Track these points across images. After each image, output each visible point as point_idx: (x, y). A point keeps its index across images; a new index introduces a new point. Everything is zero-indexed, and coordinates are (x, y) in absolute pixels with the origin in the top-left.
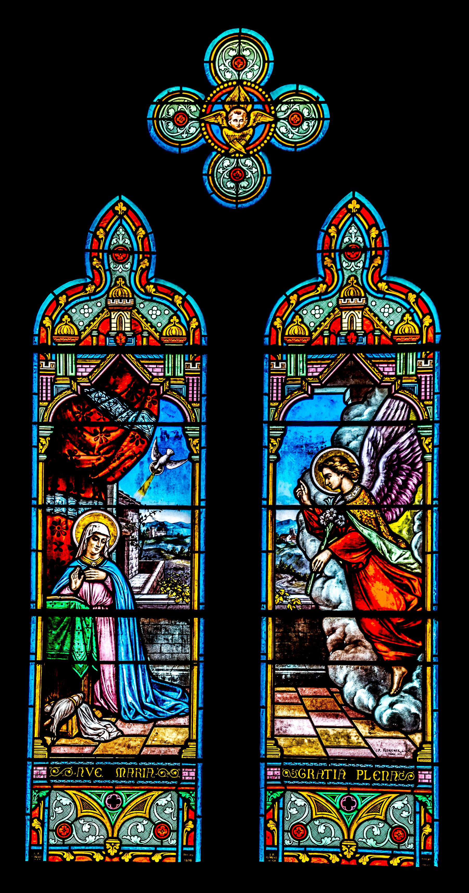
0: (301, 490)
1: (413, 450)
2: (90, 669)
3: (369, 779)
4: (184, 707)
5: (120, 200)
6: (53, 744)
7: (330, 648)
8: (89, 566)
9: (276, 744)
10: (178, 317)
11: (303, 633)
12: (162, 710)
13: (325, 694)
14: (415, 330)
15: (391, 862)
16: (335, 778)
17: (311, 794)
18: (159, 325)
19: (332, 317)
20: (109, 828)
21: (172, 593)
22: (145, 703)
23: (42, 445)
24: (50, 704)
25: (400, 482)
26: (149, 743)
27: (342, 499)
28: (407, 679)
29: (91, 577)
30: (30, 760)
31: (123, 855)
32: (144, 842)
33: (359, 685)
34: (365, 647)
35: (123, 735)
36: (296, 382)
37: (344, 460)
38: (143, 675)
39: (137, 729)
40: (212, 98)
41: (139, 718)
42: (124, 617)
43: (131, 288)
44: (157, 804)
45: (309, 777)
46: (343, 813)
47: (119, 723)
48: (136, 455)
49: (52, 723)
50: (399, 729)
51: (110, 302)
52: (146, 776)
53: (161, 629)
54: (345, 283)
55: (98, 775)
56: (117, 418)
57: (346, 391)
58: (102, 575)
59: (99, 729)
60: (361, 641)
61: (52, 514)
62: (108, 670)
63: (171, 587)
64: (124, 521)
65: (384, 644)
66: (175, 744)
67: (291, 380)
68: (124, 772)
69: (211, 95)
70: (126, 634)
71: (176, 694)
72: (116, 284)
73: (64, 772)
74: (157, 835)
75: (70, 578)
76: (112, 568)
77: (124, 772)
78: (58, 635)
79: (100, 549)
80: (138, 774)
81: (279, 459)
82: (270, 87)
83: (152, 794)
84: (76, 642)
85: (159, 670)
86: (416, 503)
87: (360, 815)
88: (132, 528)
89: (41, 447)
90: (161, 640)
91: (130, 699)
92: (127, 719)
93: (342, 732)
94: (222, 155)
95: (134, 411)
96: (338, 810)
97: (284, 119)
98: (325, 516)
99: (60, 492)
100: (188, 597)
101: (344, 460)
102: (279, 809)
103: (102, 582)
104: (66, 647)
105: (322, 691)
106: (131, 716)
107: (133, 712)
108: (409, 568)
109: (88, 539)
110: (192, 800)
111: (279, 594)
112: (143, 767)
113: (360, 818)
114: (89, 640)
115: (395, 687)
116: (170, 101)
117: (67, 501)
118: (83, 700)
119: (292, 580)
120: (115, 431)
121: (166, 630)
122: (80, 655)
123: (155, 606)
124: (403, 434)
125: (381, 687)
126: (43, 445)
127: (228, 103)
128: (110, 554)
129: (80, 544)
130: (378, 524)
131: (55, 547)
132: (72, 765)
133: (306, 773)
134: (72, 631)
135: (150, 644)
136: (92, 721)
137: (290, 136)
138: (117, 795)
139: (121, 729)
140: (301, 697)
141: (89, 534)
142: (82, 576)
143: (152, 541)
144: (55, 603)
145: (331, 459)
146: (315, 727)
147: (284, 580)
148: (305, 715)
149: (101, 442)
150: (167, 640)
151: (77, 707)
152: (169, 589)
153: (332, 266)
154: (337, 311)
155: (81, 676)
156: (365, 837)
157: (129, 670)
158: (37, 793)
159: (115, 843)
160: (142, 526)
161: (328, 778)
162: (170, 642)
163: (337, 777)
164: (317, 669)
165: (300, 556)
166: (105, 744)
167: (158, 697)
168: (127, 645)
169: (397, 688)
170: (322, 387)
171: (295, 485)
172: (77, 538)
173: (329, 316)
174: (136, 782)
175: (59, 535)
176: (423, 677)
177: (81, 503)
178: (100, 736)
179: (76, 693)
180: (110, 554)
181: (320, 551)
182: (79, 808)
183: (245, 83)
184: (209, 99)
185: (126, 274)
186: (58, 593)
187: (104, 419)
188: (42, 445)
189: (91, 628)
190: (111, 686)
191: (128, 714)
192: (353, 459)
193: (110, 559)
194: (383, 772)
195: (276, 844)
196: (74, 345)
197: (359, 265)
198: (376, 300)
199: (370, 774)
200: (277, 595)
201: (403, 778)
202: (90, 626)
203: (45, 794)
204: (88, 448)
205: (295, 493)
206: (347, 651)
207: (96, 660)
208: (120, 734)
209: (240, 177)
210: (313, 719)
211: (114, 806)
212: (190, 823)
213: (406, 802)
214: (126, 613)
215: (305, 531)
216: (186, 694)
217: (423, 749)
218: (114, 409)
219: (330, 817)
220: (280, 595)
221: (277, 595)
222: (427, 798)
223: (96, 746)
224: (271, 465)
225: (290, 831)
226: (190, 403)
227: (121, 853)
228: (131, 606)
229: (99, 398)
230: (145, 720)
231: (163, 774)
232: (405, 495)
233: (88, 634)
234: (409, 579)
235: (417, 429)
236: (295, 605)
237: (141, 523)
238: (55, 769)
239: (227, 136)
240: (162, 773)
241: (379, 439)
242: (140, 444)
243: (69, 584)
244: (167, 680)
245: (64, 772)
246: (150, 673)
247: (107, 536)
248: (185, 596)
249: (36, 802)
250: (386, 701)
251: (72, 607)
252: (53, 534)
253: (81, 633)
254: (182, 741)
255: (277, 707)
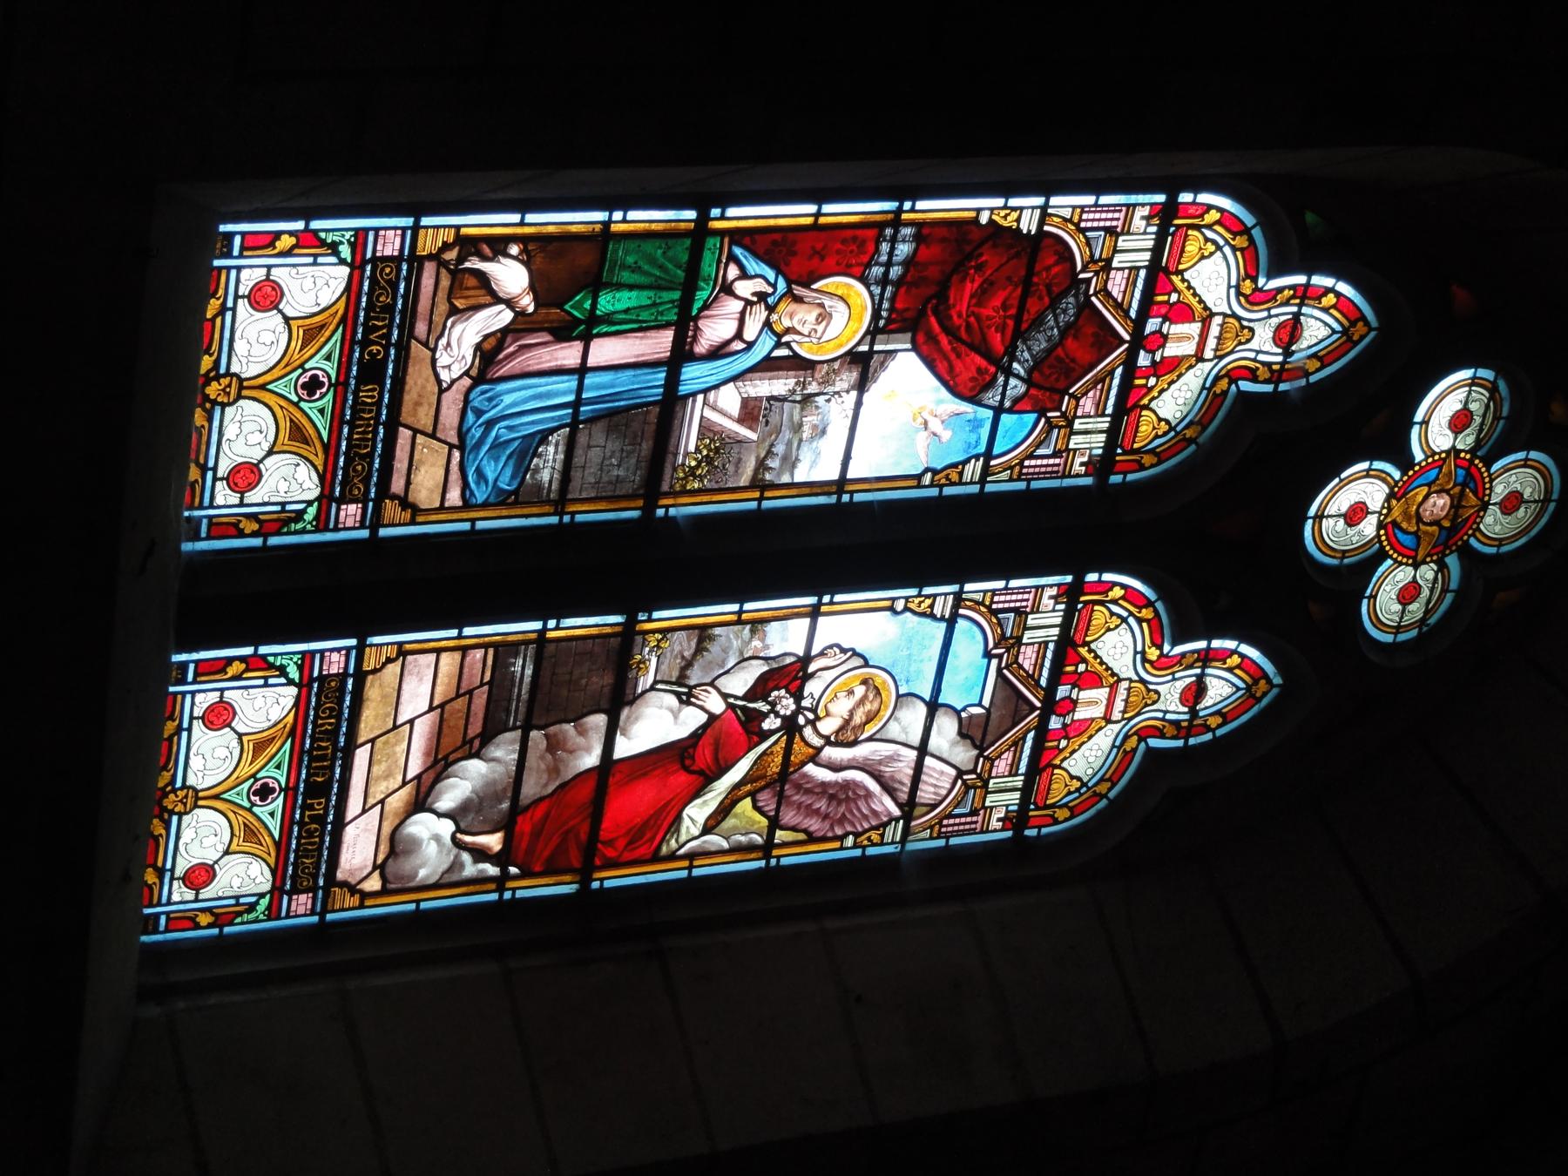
0: (835, 655)
1: (866, 817)
2: (578, 322)
3: (307, 820)
4: (480, 495)
5: (1371, 329)
6: (442, 264)
7: (552, 729)
8: (771, 309)
9: (389, 660)
10: (1165, 434)
11: (587, 685)
12: (480, 457)
13: (469, 731)
14: (1053, 798)
15: (150, 870)
16: (314, 765)
17: (287, 729)
18: (1072, 763)
19: (1105, 674)
20: (261, 381)
21: (695, 459)
22: (497, 427)
23: (1006, 215)
24: (521, 253)
25: (817, 806)
26: (420, 439)
27: (808, 722)
28: (480, 854)
29: (750, 314)
30: (417, 222)
31: (205, 410)
32: (225, 446)
33: (479, 783)
34: (546, 785)
35: (441, 391)
36: (1016, 630)
37: (870, 718)
38: (553, 419)
39: (450, 415)
40: (1476, 466)
41: (470, 417)
42: (667, 379)
43: (1232, 352)
44: (298, 465)
45: (320, 722)
46: (246, 785)
47: (467, 382)
48: (953, 378)
49: (485, 259)
50: (393, 852)
51: (1218, 320)
52: (357, 439)
53: (633, 445)
54: (1151, 687)
55: (370, 353)
56: (1024, 342)
57: (983, 707)
58: (749, 334)
59: (459, 347)
60: (557, 778)
61: (879, 238)
62: (569, 354)
63: (707, 456)
64: (842, 365)
65: (547, 815)
66: (411, 486)
67: (1020, 621)
68: (369, 400)
69: (1480, 465)
70: (633, 384)
71: (507, 480)
72: (1243, 328)
73: (384, 288)
74: (236, 470)
75: (757, 276)
76: (761, 351)
77: (369, 400)
78: (652, 261)
79: (799, 328)
80: (361, 426)
81: (896, 613)
82: (1466, 553)
83: (320, 454)
84: (634, 294)
85: (557, 445)
86: (523, 647)
87: (240, 812)
88: (826, 381)
89: (1003, 213)
90: (614, 445)
91: (508, 399)
92: (472, 396)
93: (397, 766)
94: (1391, 488)
95: (1030, 372)
96: (254, 776)
97: (1415, 576)
98: (783, 697)
99: (916, 251)
100: (684, 486)
101: (870, 718)
102: (266, 678)
103: (739, 335)
104: (626, 276)
105: (476, 728)
106: (476, 403)
107: (485, 406)
108: (672, 836)
109: (822, 305)
110: (300, 526)
111: (662, 639)
112: (376, 432)
113: (235, 813)
114: (634, 317)
115: (468, 839)
116: (1491, 404)
117: (899, 264)
118: (520, 314)
119: (683, 657)
120: (1003, 341)
121: (629, 453)
122: (607, 302)
123: (677, 433)
124: (895, 800)
125: (470, 818)
126: (1005, 217)
127: (1462, 493)
128: (788, 345)
129: (816, 291)
130: (753, 781)
131: (819, 246)
132: (395, 303)
133: (329, 717)
134: (656, 287)
135: (609, 426)
136: (477, 333)
137: (1388, 589)
138: (324, 390)
139: (454, 387)
140: (470, 692)
141: (831, 307)
142: (755, 299)
143: (796, 417)
144: (713, 253)
145: (878, 693)
146: (411, 722)
147: (685, 644)
148: (436, 703)
149: (988, 318)
150: (611, 457)
151: (509, 303)
152: (705, 452)
153: (1181, 665)
154: (1112, 680)
155: (567, 307)
156: (199, 825)
157: (564, 393)
158: (348, 241)
159: (229, 394)
160: (827, 397)
161: (315, 753)
162: (607, 462)
163: (316, 768)
164: (515, 716)
165: (722, 665)
166: (428, 361)
167: (505, 449)
168: (613, 386)
169: (466, 843)
170: (999, 670)
171: (846, 646)
172: (827, 285)
173: (1108, 668)
174: (348, 422)
175: (838, 252)
176: (480, 881)
177: (889, 289)
178: (446, 349)
179: (536, 299)
180: (788, 345)
181: (725, 696)
182: (308, 321)
183: (1410, 561)
184: (1477, 461)
185: (1254, 345)
186: (732, 258)
187: (1027, 321)
188: (1006, 215)
189: (656, 320)
190: (538, 364)
191: (480, 398)
192: (870, 730)
193: (778, 345)
194: (317, 840)
195: (198, 679)
196: (1163, 265)
197: (1173, 704)
198: (1113, 736)
199: (313, 819)
200: (660, 637)
201: (303, 872)
202: (659, 318)
203: (343, 256)
204: (981, 296)
205: (831, 647)
206: (542, 758)
207: (595, 331)
208: (445, 385)
209: (1351, 519)
210: (428, 715)
211: (304, 386)
212: (256, 526)
213: (257, 881)
214: (673, 381)
215: (766, 668)
216: (504, 500)
217: (352, 895)
218: (1040, 336)
219: (242, 764)
220: (659, 641)
221: (660, 637)
222: (263, 913)
223: (426, 344)
224: (888, 603)
225: (221, 700)
226: (1022, 462)
227: (208, 405)
228: (684, 389)
229: (1065, 311)
230: (464, 429)
231: (355, 470)
232: (795, 815)
233: (644, 316)
234: (652, 839)
235: (897, 820)
236: (638, 667)
237: (833, 396)
238: (391, 272)
239: (1417, 494)
240: (359, 468)
241: (895, 765)
242: (971, 384)
243: (744, 275)
244: (535, 460)
245: (384, 288)
246: (552, 431)
247: (820, 339)
248: (687, 482)
249: (329, 241)
250: (447, 827)
251: (702, 284)
252: (844, 241)
253: (649, 302)
254: (415, 498)
255: (457, 656)
